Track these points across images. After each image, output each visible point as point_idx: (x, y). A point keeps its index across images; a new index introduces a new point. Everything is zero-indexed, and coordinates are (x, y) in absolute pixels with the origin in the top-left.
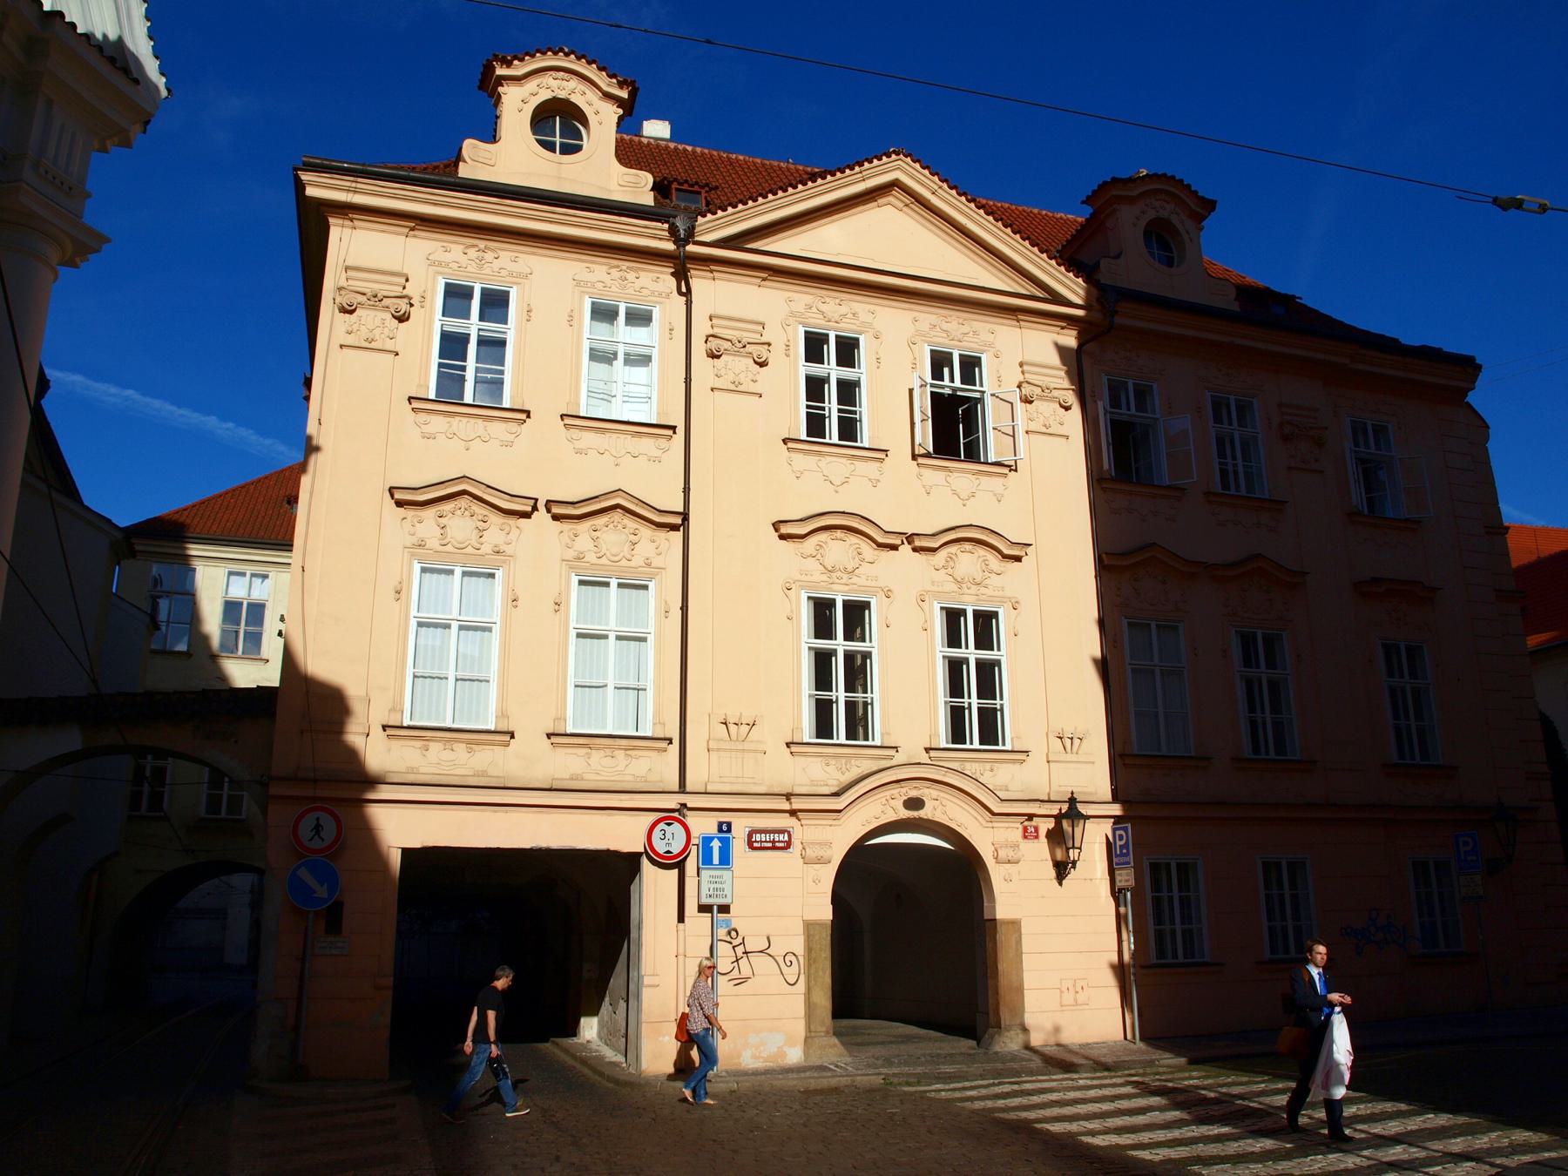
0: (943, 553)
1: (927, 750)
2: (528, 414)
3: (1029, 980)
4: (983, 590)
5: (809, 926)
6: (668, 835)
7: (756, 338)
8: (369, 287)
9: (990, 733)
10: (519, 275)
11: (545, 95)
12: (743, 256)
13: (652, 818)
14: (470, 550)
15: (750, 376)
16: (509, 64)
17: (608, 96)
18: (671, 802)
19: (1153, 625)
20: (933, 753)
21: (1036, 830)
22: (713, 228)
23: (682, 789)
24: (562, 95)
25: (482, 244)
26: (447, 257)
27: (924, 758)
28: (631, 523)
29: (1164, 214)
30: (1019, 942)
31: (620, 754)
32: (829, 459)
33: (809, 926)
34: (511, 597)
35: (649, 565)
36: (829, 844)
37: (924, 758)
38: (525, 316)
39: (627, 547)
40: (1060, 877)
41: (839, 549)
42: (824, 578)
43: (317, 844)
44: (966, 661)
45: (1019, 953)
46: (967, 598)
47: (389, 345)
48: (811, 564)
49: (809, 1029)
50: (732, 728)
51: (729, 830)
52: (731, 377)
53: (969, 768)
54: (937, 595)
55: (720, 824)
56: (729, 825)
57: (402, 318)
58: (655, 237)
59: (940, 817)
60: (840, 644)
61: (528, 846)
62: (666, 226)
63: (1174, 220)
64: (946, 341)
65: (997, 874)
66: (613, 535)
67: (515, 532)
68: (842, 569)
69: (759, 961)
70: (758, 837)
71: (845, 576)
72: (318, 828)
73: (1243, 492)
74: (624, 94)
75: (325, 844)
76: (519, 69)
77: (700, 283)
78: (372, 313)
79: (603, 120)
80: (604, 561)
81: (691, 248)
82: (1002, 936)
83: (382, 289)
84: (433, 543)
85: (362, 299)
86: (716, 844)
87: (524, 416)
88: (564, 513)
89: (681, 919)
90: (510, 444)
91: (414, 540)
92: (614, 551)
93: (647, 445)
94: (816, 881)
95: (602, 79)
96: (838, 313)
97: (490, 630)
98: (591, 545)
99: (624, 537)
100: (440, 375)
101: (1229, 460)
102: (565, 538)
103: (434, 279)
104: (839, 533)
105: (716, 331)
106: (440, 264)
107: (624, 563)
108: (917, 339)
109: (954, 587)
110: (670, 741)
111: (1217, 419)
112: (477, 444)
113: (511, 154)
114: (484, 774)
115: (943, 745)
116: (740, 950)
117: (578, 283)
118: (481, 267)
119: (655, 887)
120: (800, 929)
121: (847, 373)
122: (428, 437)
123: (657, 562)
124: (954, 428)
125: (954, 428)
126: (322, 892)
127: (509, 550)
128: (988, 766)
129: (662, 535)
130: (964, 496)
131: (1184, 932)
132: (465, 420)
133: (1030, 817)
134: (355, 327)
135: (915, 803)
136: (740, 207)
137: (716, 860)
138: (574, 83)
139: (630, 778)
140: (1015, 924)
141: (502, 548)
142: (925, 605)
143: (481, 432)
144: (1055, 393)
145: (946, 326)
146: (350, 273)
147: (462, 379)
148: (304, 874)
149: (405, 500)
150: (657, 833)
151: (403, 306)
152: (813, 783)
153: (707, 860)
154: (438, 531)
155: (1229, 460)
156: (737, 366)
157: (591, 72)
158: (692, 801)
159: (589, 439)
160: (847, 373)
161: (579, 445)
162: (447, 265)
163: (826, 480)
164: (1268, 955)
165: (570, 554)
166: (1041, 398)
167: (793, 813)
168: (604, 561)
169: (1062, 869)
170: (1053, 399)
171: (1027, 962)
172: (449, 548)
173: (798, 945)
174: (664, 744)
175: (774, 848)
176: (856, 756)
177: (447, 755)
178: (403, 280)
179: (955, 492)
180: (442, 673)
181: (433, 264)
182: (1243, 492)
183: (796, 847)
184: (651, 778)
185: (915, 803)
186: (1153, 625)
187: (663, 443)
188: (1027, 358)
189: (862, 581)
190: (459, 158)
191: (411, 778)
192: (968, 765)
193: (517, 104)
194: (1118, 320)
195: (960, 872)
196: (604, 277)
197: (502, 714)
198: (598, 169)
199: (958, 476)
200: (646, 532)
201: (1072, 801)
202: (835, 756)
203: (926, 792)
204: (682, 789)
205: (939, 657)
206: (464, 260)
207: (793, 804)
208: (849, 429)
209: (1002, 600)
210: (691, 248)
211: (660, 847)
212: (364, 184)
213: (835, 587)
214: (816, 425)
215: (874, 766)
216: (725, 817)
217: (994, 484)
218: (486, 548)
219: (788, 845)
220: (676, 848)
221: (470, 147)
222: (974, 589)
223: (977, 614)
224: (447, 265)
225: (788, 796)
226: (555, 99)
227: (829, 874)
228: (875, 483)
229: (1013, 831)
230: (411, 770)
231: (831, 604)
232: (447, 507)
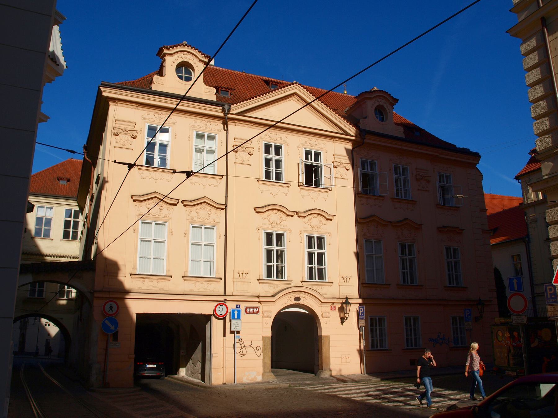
0: (307, 218)
1: (301, 282)
4: (279, 226)
5: (264, 338)
7: (132, 128)
8: (123, 127)
11: (180, 60)
14: (157, 216)
16: (168, 49)
17: (201, 61)
19: (373, 241)
20: (303, 283)
21: (335, 307)
22: (236, 109)
23: (225, 294)
24: (186, 60)
25: (160, 112)
28: (209, 207)
29: (381, 103)
33: (264, 338)
37: (300, 284)
41: (275, 216)
43: (111, 312)
44: (273, 250)
46: (314, 233)
47: (130, 147)
48: (307, 225)
55: (237, 306)
56: (239, 306)
58: (217, 111)
61: (142, 313)
63: (385, 105)
64: (271, 140)
65: (322, 321)
66: (203, 212)
68: (276, 223)
69: (249, 349)
70: (248, 310)
72: (111, 307)
73: (403, 198)
74: (206, 60)
75: (114, 312)
76: (172, 51)
78: (124, 136)
81: (229, 116)
83: (128, 128)
85: (121, 131)
88: (187, 204)
89: (224, 335)
90: (169, 181)
93: (214, 181)
96: (274, 137)
97: (164, 242)
101: (399, 187)
104: (275, 211)
105: (336, 159)
107: (206, 220)
109: (311, 229)
111: (396, 173)
113: (169, 82)
114: (162, 289)
115: (307, 280)
116: (243, 345)
117: (191, 126)
119: (217, 325)
121: (278, 157)
123: (217, 220)
124: (312, 176)
125: (312, 176)
126: (113, 328)
129: (219, 211)
131: (380, 340)
133: (333, 303)
135: (297, 299)
137: (516, 288)
138: (190, 56)
140: (328, 337)
141: (167, 215)
142: (302, 235)
145: (271, 135)
148: (107, 322)
150: (217, 309)
153: (234, 317)
155: (399, 187)
157: (193, 51)
158: (228, 298)
160: (278, 157)
162: (149, 119)
163: (271, 193)
164: (406, 347)
165: (189, 218)
166: (340, 166)
167: (259, 302)
168: (200, 220)
169: (343, 320)
170: (343, 167)
173: (261, 344)
175: (253, 313)
176: (279, 284)
177: (151, 283)
180: (148, 256)
181: (144, 119)
182: (403, 198)
186: (373, 241)
190: (151, 82)
193: (171, 63)
194: (365, 141)
196: (200, 124)
197: (168, 270)
199: (313, 192)
201: (347, 298)
203: (301, 295)
204: (225, 294)
205: (306, 251)
206: (154, 117)
207: (260, 300)
208: (278, 176)
211: (218, 313)
212: (122, 92)
214: (268, 175)
216: (238, 303)
217: (285, 190)
218: (162, 216)
219: (258, 312)
220: (223, 313)
221: (156, 78)
226: (184, 62)
228: (286, 194)
229: (327, 308)
231: (272, 234)
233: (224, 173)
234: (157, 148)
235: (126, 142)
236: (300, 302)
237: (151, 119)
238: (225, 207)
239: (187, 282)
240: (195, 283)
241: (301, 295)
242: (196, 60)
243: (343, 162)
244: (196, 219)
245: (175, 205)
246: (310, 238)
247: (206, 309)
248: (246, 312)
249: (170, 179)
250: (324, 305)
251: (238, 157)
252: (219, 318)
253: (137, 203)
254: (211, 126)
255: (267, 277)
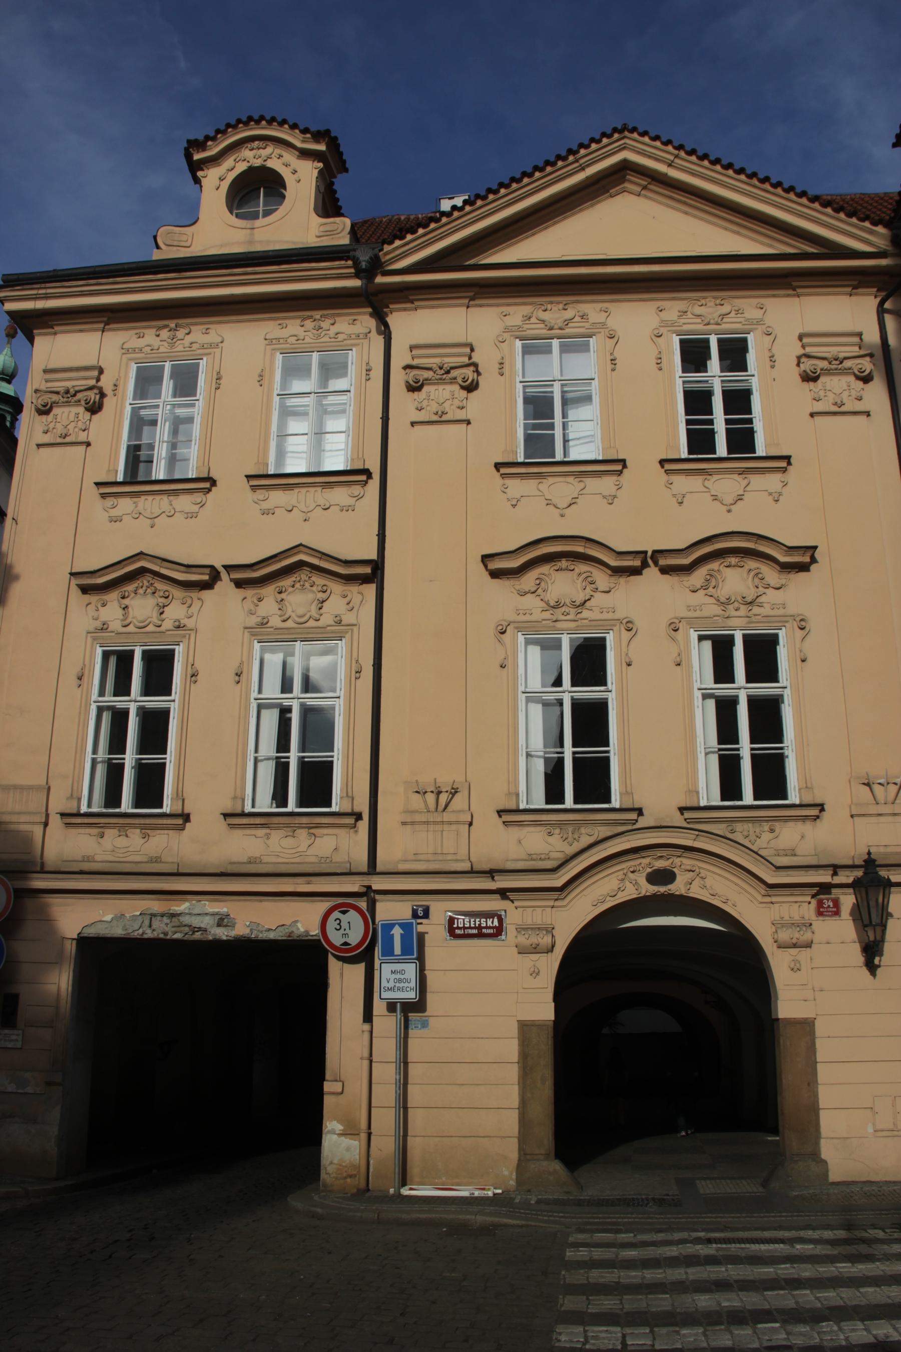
0: (701, 573)
1: (682, 810)
2: (623, 462)
3: (826, 1096)
4: (756, 610)
5: (525, 1027)
6: (344, 924)
8: (60, 386)
9: (771, 777)
10: (212, 346)
11: (242, 167)
12: (464, 276)
13: (323, 906)
14: (151, 628)
15: (457, 403)
17: (305, 154)
18: (352, 885)
20: (687, 815)
21: (836, 903)
24: (258, 163)
26: (140, 343)
27: (678, 820)
28: (319, 580)
30: (812, 1048)
31: (302, 834)
32: (551, 480)
33: (525, 1027)
34: (190, 672)
35: (339, 623)
36: (550, 930)
37: (678, 820)
38: (609, 367)
39: (314, 607)
40: (872, 968)
41: (735, 579)
42: (547, 615)
45: (812, 1064)
47: (859, 406)
48: (531, 602)
49: (522, 1152)
50: (876, 788)
51: (426, 915)
52: (434, 407)
53: (741, 832)
54: (691, 622)
57: (471, 387)
59: (697, 892)
60: (135, 701)
62: (350, 263)
64: (700, 327)
65: (779, 964)
66: (299, 599)
67: (197, 604)
68: (138, 615)
71: (573, 611)
74: (322, 147)
76: (214, 150)
77: (398, 320)
78: (66, 410)
79: (302, 178)
80: (290, 624)
81: (379, 279)
82: (787, 1043)
84: (115, 625)
85: (55, 398)
86: (397, 932)
87: (783, 464)
89: (368, 1017)
90: (192, 516)
91: (98, 624)
92: (300, 611)
93: (340, 495)
94: (535, 973)
95: (296, 139)
98: (276, 606)
99: (311, 596)
100: (689, 432)
102: (248, 605)
103: (127, 366)
104: (564, 563)
105: (808, 350)
106: (134, 350)
107: (312, 623)
108: (662, 330)
109: (717, 610)
110: (358, 816)
112: (162, 520)
118: (172, 345)
119: (344, 983)
120: (514, 1031)
122: (114, 520)
123: (348, 618)
124: (719, 431)
125: (719, 431)
127: (190, 623)
128: (766, 827)
129: (354, 589)
130: (729, 500)
132: (150, 498)
133: (825, 888)
134: (51, 426)
135: (663, 876)
136: (421, 231)
137: (397, 949)
139: (313, 859)
140: (807, 1026)
141: (184, 621)
142: (679, 635)
143: (321, 501)
144: (848, 364)
145: (698, 310)
146: (415, 352)
147: (712, 433)
149: (499, 568)
150: (331, 924)
151: (93, 396)
152: (531, 857)
153: (388, 951)
154: (120, 612)
156: (441, 395)
158: (378, 884)
159: (278, 498)
161: (265, 505)
162: (286, 340)
165: (253, 621)
166: (828, 372)
167: (503, 893)
168: (290, 624)
169: (872, 952)
171: (823, 1073)
172: (131, 629)
174: (350, 821)
175: (480, 935)
176: (586, 823)
177: (122, 842)
178: (468, 350)
179: (715, 498)
181: (128, 351)
183: (510, 934)
184: (337, 858)
185: (663, 876)
187: (357, 490)
188: (808, 329)
189: (595, 615)
190: (353, 232)
191: (86, 866)
192: (739, 827)
195: (736, 960)
198: (296, 222)
200: (336, 587)
201: (870, 864)
202: (560, 825)
203: (680, 864)
206: (156, 342)
207: (498, 882)
208: (742, 440)
209: (783, 621)
210: (379, 279)
211: (336, 939)
213: (559, 625)
214: (700, 441)
215: (605, 831)
217: (772, 481)
218: (168, 625)
219: (498, 931)
222: (743, 610)
223: (747, 639)
224: (286, 342)
225: (491, 873)
226: (251, 170)
227: (550, 965)
228: (611, 499)
229: (802, 908)
230: (87, 859)
232: (286, 582)
233: (375, 467)
234: (718, 402)
235: (71, 427)
236: (678, 887)
237: (148, 349)
238: (373, 573)
239: (239, 832)
240: (268, 836)
241: (678, 861)
242: (289, 157)
243: (842, 355)
244: (275, 622)
245: (803, 568)
246: (722, 649)
247: (304, 920)
248: (452, 931)
249: (195, 508)
250: (779, 898)
251: (425, 404)
252: (364, 955)
253: (250, 593)
254: (334, 330)
255: (107, 806)
